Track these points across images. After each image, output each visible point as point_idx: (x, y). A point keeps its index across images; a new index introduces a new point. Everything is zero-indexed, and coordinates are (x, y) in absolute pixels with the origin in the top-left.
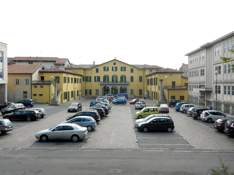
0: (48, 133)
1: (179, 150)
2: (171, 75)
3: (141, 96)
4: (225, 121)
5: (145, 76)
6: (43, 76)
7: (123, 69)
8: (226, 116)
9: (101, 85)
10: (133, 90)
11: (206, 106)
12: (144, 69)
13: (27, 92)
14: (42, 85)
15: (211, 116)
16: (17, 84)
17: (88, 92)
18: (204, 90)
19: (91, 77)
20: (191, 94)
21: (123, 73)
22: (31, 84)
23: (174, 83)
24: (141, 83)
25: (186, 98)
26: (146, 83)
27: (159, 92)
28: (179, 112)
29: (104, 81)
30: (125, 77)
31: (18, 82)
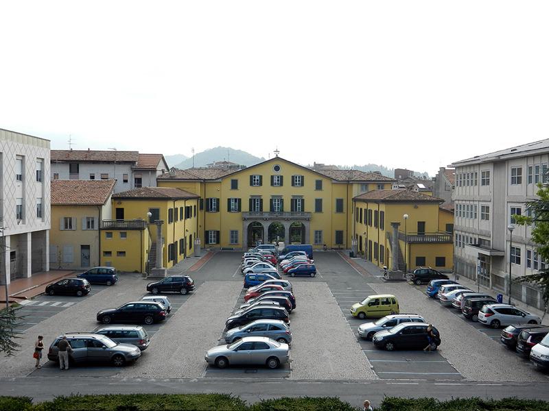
0: (227, 354)
1: (442, 382)
2: (416, 207)
3: (341, 247)
4: (518, 331)
5: (350, 201)
6: (120, 207)
7: (297, 181)
8: (525, 315)
9: (245, 219)
10: (320, 232)
11: (492, 285)
12: (348, 181)
15: (498, 315)
16: (66, 227)
18: (488, 253)
19: (218, 200)
20: (460, 255)
21: (298, 191)
22: (100, 229)
23: (421, 225)
24: (339, 215)
25: (449, 263)
26: (353, 216)
27: (388, 246)
28: (435, 301)
29: (250, 210)
30: (303, 201)
31: (68, 224)
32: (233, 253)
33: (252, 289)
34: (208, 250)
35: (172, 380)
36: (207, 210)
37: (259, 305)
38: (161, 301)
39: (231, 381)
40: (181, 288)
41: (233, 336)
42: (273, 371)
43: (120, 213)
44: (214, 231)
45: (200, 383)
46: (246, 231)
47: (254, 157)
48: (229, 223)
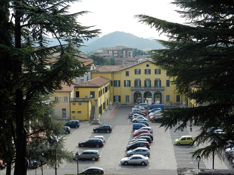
0: (127, 160)
3: (179, 103)
6: (78, 91)
9: (132, 90)
10: (169, 96)
13: (66, 109)
14: (81, 103)
17: (116, 99)
19: (119, 81)
22: (70, 102)
29: (135, 86)
30: (160, 81)
32: (126, 107)
33: (136, 131)
34: (115, 105)
35: (110, 169)
36: (115, 86)
37: (139, 140)
38: (98, 137)
39: (129, 170)
40: (106, 130)
41: (129, 153)
42: (143, 166)
43: (77, 94)
44: (118, 96)
45: (119, 170)
46: (133, 96)
47: (137, 37)
48: (125, 92)
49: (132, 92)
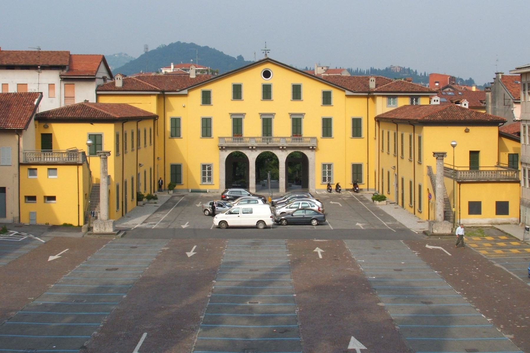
10: (330, 166)
22: (20, 164)
23: (474, 155)
24: (357, 141)
49: (220, 156)
